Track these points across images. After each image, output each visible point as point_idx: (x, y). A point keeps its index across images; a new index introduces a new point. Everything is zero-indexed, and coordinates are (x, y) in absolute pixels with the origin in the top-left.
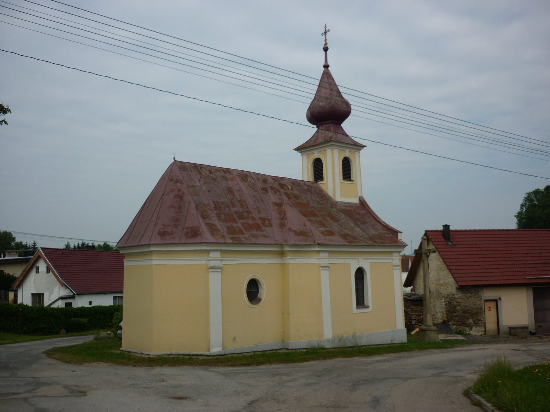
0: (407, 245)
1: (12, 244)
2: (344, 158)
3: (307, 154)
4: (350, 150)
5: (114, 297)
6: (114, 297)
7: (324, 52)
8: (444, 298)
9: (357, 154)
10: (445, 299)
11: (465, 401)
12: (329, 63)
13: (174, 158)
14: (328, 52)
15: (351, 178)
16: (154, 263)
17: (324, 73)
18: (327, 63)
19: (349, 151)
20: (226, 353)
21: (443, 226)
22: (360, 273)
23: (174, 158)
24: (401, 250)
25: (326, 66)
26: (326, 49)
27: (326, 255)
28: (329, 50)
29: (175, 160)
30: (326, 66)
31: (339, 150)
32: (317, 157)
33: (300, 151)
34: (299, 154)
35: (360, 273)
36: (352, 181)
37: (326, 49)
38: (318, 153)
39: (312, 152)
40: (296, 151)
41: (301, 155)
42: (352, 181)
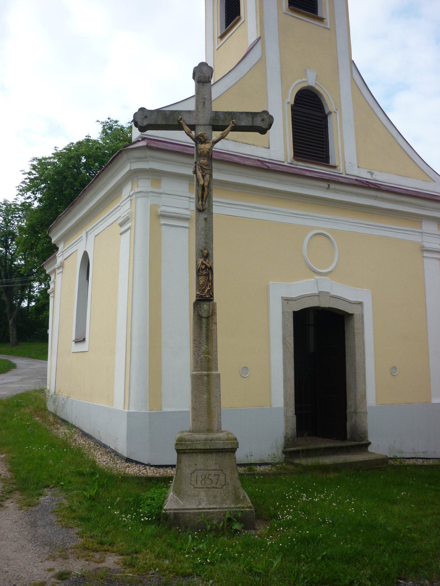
36: (321, 19)
42: (321, 19)
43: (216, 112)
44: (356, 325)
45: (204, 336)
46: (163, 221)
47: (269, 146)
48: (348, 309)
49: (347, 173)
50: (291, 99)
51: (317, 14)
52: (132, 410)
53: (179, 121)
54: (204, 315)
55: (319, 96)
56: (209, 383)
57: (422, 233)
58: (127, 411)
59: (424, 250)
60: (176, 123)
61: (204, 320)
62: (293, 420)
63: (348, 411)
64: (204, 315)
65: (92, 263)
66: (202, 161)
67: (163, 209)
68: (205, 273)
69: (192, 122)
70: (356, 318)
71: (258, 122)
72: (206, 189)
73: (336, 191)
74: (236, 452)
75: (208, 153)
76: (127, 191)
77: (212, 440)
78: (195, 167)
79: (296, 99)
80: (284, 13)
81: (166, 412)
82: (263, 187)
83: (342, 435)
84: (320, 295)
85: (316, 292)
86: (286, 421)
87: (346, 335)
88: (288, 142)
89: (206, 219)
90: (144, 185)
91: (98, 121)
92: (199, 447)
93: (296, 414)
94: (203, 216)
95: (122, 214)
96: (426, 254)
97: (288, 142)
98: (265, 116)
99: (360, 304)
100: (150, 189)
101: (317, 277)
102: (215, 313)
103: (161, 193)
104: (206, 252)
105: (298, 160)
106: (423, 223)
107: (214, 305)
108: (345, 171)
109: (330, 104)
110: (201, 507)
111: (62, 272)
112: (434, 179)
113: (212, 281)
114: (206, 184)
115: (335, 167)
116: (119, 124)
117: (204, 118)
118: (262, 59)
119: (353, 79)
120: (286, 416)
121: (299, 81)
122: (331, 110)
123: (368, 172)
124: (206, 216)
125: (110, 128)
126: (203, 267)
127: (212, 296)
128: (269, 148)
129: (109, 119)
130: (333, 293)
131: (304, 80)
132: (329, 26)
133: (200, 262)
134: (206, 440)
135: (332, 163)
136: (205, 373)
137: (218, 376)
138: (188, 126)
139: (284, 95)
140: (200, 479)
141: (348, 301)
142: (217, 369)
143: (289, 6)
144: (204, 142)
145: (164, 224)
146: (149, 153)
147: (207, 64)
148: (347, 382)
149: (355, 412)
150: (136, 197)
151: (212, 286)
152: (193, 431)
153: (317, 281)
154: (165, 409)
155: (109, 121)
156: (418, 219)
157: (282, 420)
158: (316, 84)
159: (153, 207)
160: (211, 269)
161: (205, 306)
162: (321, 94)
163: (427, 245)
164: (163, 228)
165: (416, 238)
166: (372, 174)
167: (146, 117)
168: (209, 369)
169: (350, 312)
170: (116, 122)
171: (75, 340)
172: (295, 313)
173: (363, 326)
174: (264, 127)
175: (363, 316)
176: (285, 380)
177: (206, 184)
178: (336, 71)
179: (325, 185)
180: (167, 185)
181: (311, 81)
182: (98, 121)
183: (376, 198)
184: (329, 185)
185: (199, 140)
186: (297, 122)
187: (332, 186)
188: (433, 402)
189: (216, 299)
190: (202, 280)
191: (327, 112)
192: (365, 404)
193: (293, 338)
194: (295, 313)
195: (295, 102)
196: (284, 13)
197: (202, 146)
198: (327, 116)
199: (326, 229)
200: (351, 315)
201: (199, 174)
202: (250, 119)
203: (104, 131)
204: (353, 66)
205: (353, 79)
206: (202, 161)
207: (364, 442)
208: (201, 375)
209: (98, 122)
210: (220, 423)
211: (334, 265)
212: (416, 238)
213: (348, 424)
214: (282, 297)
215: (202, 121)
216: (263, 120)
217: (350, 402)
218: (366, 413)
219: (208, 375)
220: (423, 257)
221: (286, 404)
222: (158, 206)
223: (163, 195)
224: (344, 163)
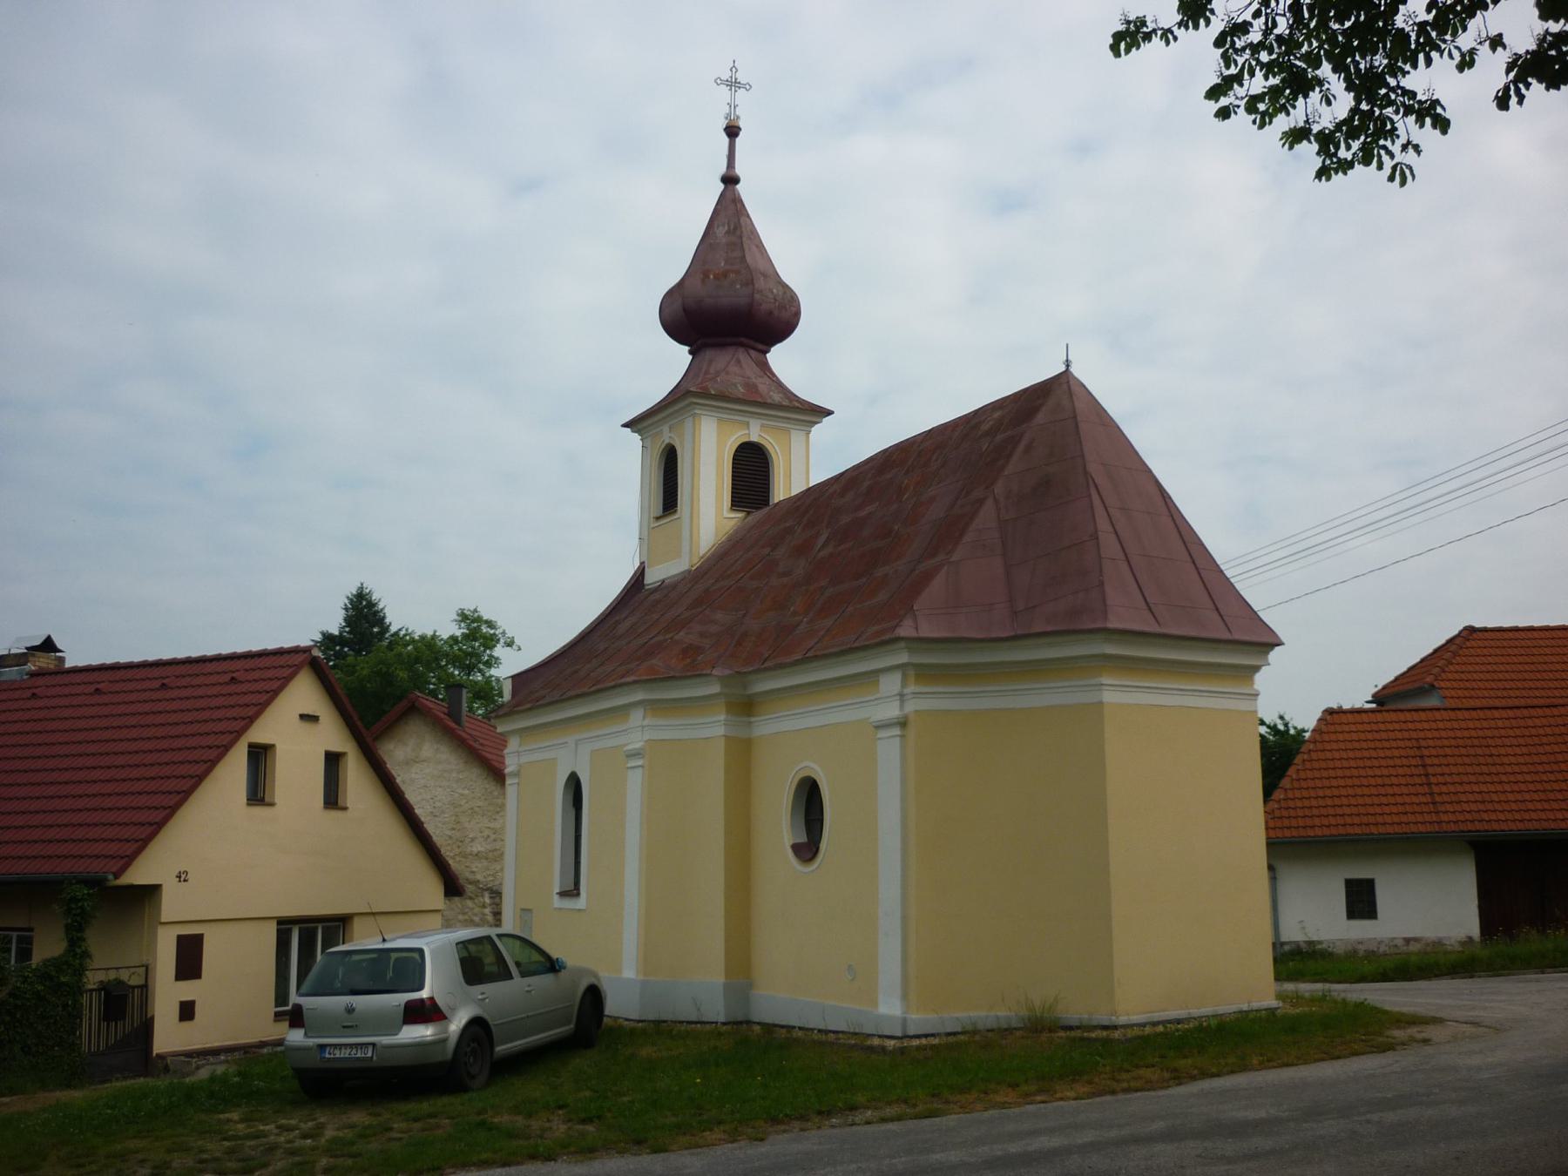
0: (1280, 644)
4: (764, 422)
5: (179, 937)
6: (179, 937)
7: (726, 140)
8: (487, 895)
9: (796, 437)
10: (491, 898)
12: (739, 170)
13: (1068, 363)
16: (1110, 697)
23: (1068, 363)
24: (1259, 663)
25: (730, 180)
26: (732, 131)
28: (741, 134)
29: (1067, 370)
30: (730, 180)
31: (720, 420)
32: (667, 441)
34: (637, 437)
37: (732, 131)
39: (747, 419)
41: (642, 440)
76: (636, 717)
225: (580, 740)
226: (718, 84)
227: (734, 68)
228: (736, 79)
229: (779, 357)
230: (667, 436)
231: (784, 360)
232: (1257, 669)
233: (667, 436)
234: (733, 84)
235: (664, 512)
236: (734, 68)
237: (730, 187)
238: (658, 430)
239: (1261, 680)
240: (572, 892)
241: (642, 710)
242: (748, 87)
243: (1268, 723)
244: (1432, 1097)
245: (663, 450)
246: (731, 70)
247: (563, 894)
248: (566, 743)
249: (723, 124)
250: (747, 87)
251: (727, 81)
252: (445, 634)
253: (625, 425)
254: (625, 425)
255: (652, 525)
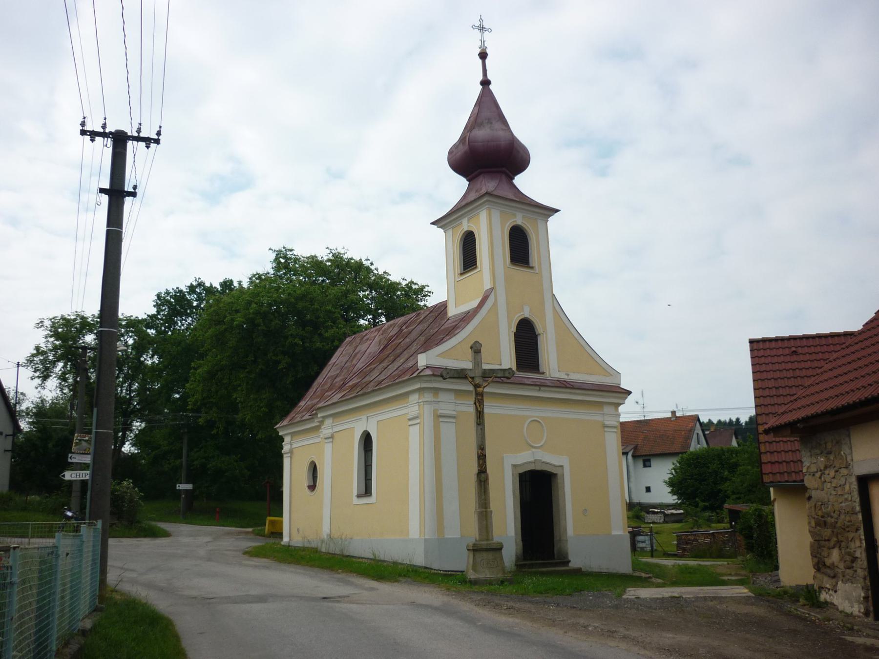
1: (129, 352)
2: (521, 320)
3: (453, 228)
4: (524, 214)
7: (480, 61)
9: (540, 223)
11: (390, 273)
14: (487, 61)
15: (529, 263)
17: (480, 102)
18: (487, 78)
19: (523, 217)
20: (386, 559)
21: (710, 420)
22: (367, 440)
25: (486, 83)
26: (483, 56)
27: (450, 397)
30: (486, 83)
32: (466, 229)
33: (440, 225)
34: (441, 231)
35: (367, 440)
36: (532, 268)
37: (483, 56)
38: (468, 223)
40: (435, 227)
42: (532, 268)
43: (485, 369)
44: (559, 481)
45: (483, 491)
46: (441, 420)
47: (501, 363)
48: (554, 471)
49: (551, 376)
50: (514, 329)
51: (529, 265)
52: (426, 537)
53: (465, 375)
54: (483, 480)
55: (532, 323)
56: (486, 516)
57: (603, 414)
58: (423, 538)
59: (605, 427)
60: (464, 376)
61: (483, 483)
62: (521, 544)
63: (555, 539)
64: (483, 480)
65: (376, 439)
66: (479, 397)
67: (440, 411)
68: (482, 458)
69: (472, 376)
70: (559, 477)
71: (507, 375)
72: (481, 413)
73: (545, 391)
74: (502, 551)
75: (482, 393)
76: (414, 398)
77: (490, 544)
78: (475, 400)
79: (518, 327)
80: (509, 268)
81: (447, 538)
82: (549, 472)
83: (551, 555)
84: (535, 462)
85: (532, 460)
86: (517, 545)
87: (553, 488)
88: (513, 360)
89: (481, 429)
90: (428, 397)
91: (270, 249)
92: (484, 547)
93: (522, 540)
94: (480, 427)
95: (411, 412)
96: (606, 429)
97: (513, 360)
98: (510, 371)
99: (562, 466)
100: (433, 400)
101: (534, 450)
102: (488, 479)
103: (439, 402)
104: (482, 446)
105: (519, 371)
106: (604, 407)
107: (488, 475)
108: (550, 375)
109: (539, 328)
110: (487, 576)
111: (332, 442)
112: (611, 373)
113: (486, 462)
114: (481, 410)
115: (543, 373)
116: (294, 253)
117: (478, 373)
118: (495, 304)
119: (554, 308)
120: (516, 542)
121: (519, 314)
122: (540, 333)
123: (566, 374)
124: (481, 427)
125: (285, 257)
126: (482, 455)
127: (486, 470)
128: (501, 365)
129: (284, 248)
130: (544, 460)
131: (522, 313)
132: (537, 272)
133: (480, 452)
134: (487, 544)
135: (541, 371)
136: (484, 510)
137: (491, 511)
138: (470, 377)
139: (510, 326)
140: (485, 563)
141: (528, 387)
142: (490, 508)
143: (511, 262)
144: (479, 387)
145: (442, 421)
146: (433, 378)
147: (479, 342)
148: (554, 520)
149: (560, 540)
150: (424, 404)
151: (486, 465)
152: (480, 540)
153: (533, 453)
154: (446, 536)
155: (283, 250)
156: (601, 404)
157: (514, 544)
158: (530, 315)
159: (435, 411)
160: (485, 455)
161: (483, 475)
162: (533, 322)
163: (607, 423)
164: (441, 423)
165: (598, 418)
166: (568, 375)
167: (448, 373)
168: (486, 508)
169: (555, 472)
170: (291, 250)
171: (357, 495)
172: (519, 474)
173: (564, 481)
174: (510, 377)
175: (563, 475)
176: (515, 518)
177: (481, 410)
178: (542, 303)
179: (538, 388)
180: (442, 396)
181: (526, 314)
182: (270, 249)
183: (571, 393)
184: (540, 388)
185: (476, 386)
186: (519, 348)
187: (542, 388)
188: (613, 534)
189: (488, 471)
190: (481, 462)
191: (537, 334)
192: (566, 534)
193: (519, 491)
194: (519, 474)
195: (517, 329)
196: (509, 268)
197: (478, 389)
198: (537, 336)
199: (537, 417)
200: (555, 475)
201: (478, 404)
202: (503, 372)
203: (276, 259)
204: (555, 300)
205: (554, 308)
206: (479, 397)
207: (566, 560)
208: (483, 511)
209: (271, 251)
210: (492, 536)
211: (544, 441)
212: (598, 418)
213: (556, 549)
214: (512, 465)
215: (477, 375)
216: (509, 373)
217: (556, 534)
218: (567, 540)
219: (486, 511)
220: (605, 431)
221: (516, 534)
222: (437, 410)
223: (440, 403)
224: (549, 369)
225: (369, 416)
226: (473, 29)
227: (481, 20)
228: (481, 32)
229: (520, 181)
230: (465, 225)
231: (523, 182)
232: (620, 404)
233: (465, 225)
234: (482, 29)
235: (464, 269)
236: (481, 20)
237: (486, 86)
238: (459, 222)
239: (621, 409)
240: (367, 491)
241: (332, 419)
242: (490, 30)
243: (701, 421)
244: (479, 598)
245: (464, 234)
246: (479, 21)
247: (359, 496)
248: (361, 418)
249: (479, 51)
250: (489, 30)
251: (478, 27)
252: (66, 472)
253: (433, 223)
254: (433, 223)
255: (457, 280)
